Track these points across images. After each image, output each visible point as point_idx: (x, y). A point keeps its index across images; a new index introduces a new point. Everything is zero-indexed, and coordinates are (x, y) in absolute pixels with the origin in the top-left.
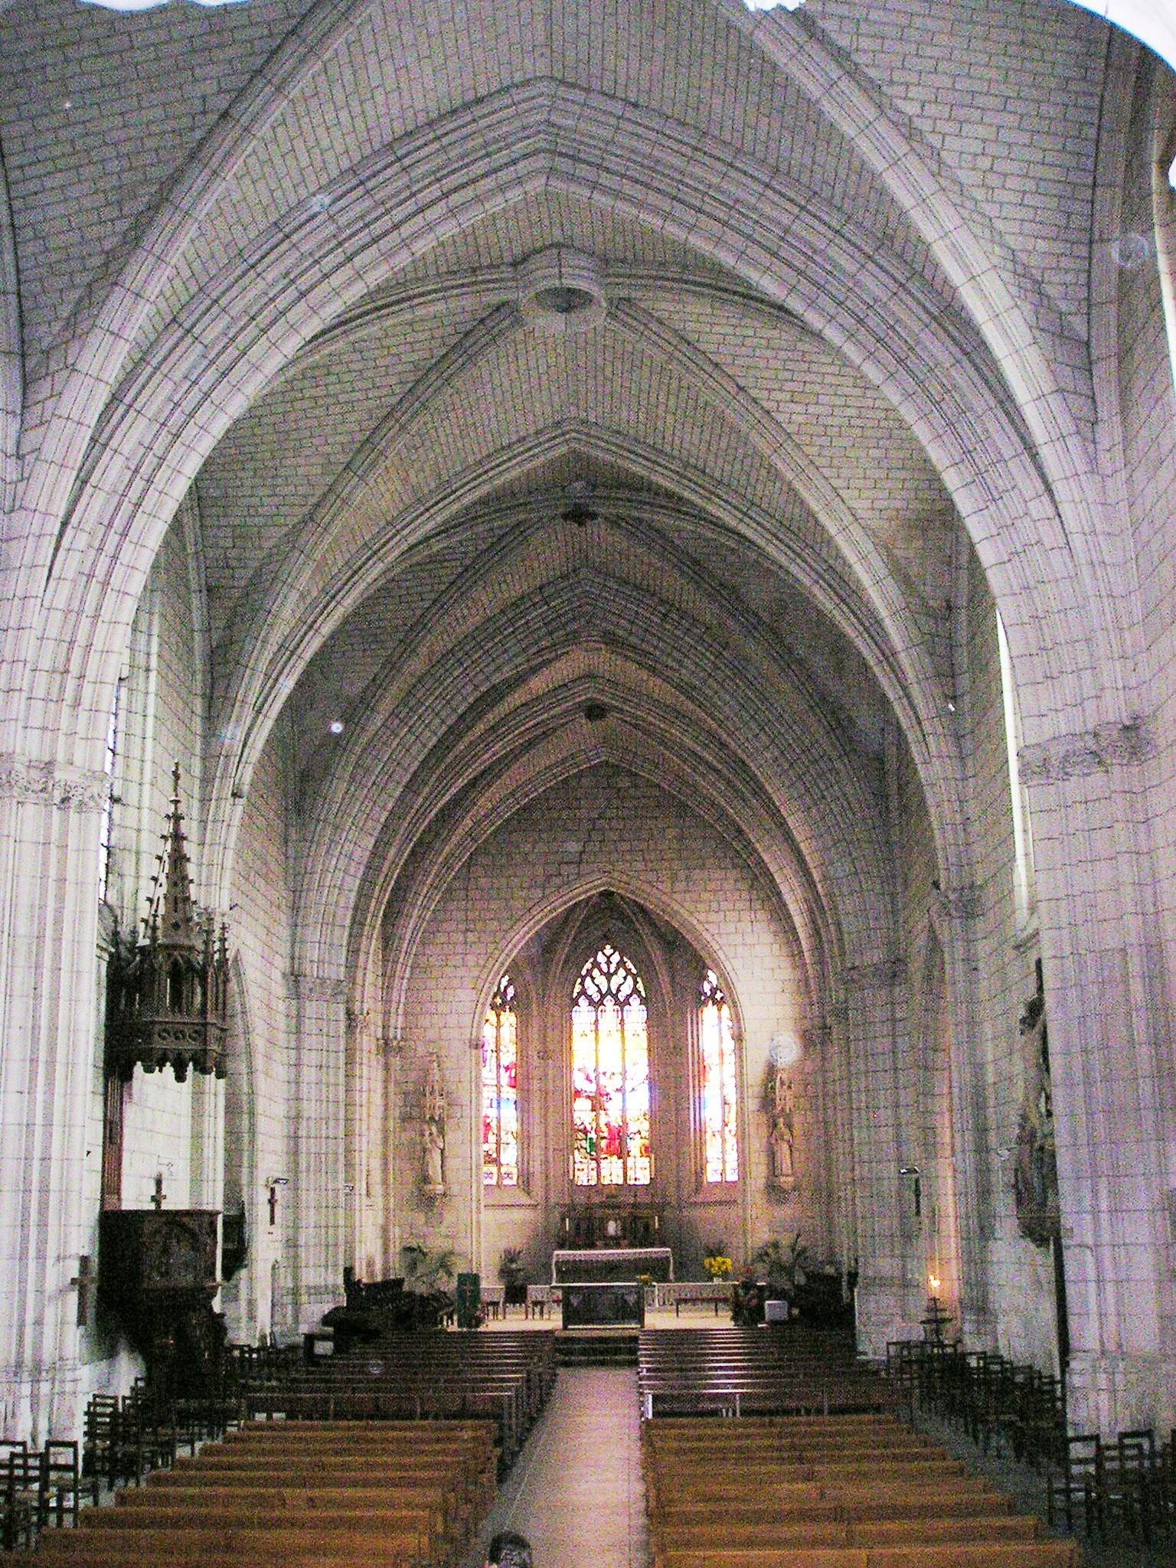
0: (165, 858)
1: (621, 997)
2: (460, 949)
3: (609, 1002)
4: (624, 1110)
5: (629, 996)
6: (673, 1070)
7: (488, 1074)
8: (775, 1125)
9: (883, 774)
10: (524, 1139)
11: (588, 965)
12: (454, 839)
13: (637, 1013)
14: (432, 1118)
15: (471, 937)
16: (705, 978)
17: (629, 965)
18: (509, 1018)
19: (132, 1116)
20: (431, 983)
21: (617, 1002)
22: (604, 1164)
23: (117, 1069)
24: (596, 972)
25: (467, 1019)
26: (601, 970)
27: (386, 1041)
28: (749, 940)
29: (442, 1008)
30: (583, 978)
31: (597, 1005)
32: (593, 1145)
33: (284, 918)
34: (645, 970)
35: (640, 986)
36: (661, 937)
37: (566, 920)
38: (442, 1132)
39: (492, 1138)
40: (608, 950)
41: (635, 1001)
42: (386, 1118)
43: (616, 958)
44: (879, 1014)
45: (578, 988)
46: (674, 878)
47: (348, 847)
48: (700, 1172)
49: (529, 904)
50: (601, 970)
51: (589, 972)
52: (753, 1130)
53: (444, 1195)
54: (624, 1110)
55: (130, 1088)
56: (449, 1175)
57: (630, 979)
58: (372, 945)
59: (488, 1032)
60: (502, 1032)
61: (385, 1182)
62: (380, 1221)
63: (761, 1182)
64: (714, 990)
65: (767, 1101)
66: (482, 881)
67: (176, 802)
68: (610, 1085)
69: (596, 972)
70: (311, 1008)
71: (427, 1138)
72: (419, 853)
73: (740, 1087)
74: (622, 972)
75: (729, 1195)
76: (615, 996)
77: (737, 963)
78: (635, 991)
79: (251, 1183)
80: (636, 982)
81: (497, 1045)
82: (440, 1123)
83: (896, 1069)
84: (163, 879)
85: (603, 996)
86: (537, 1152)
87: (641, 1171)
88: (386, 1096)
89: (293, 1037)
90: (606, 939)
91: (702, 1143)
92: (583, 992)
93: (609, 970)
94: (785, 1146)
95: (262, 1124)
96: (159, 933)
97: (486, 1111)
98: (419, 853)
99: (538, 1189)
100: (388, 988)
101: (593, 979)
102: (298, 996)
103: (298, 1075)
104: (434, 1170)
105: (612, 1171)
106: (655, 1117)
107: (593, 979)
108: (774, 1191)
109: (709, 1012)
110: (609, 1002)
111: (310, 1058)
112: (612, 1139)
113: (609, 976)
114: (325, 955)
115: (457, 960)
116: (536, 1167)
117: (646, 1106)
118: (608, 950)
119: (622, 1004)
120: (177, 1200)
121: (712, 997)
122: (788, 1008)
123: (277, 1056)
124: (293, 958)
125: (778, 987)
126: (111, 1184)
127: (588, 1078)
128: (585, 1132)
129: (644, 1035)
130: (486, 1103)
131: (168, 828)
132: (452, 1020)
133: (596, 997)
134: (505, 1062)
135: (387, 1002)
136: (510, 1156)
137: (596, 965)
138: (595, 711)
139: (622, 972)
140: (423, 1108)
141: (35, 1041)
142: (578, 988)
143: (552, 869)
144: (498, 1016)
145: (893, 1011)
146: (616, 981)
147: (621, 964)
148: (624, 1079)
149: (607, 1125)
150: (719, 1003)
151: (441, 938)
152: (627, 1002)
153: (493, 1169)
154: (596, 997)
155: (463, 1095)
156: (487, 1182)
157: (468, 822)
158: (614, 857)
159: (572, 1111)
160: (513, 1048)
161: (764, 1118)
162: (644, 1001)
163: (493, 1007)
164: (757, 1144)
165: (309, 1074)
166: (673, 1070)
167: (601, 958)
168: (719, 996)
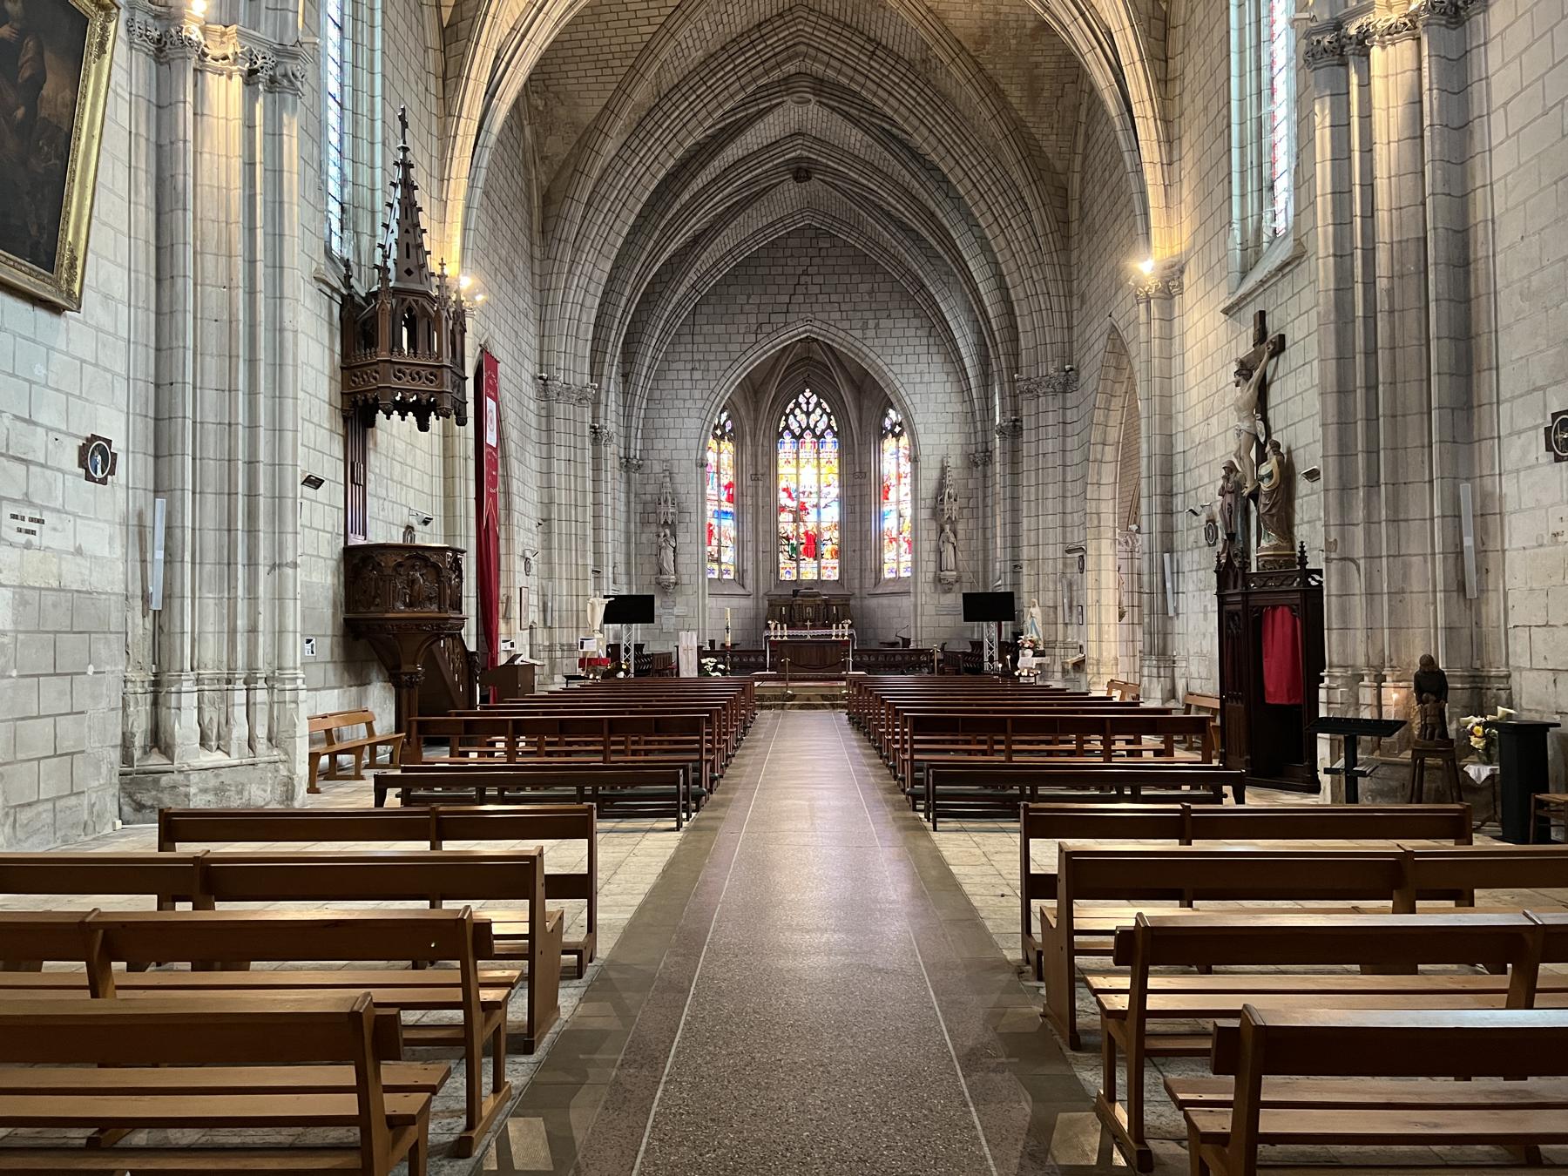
0: (396, 205)
2: (689, 347)
3: (808, 437)
4: (819, 522)
7: (711, 490)
8: (942, 530)
9: (1065, 206)
10: (740, 544)
11: (791, 405)
12: (682, 290)
13: (830, 445)
15: (697, 375)
16: (887, 415)
17: (825, 405)
18: (728, 447)
19: (376, 462)
20: (664, 413)
21: (814, 435)
22: (802, 564)
23: (357, 416)
24: (797, 411)
25: (695, 442)
27: (628, 459)
28: (926, 378)
30: (787, 416)
31: (798, 438)
32: (794, 549)
33: (532, 329)
34: (838, 411)
35: (833, 423)
36: (851, 380)
37: (774, 366)
38: (674, 535)
39: (714, 542)
40: (808, 393)
41: (829, 438)
42: (628, 521)
43: (814, 399)
44: (1051, 418)
45: (783, 424)
46: (864, 328)
47: (589, 268)
48: (879, 571)
49: (745, 347)
51: (792, 411)
52: (924, 534)
54: (819, 522)
55: (374, 436)
56: (681, 569)
58: (612, 371)
59: (711, 457)
60: (722, 456)
61: (628, 573)
63: (931, 575)
64: (894, 425)
65: (937, 512)
66: (706, 329)
67: (405, 150)
68: (810, 502)
69: (797, 411)
70: (560, 409)
71: (662, 539)
72: (649, 301)
73: (915, 500)
74: (819, 411)
75: (901, 589)
76: (813, 431)
77: (916, 399)
78: (829, 427)
79: (508, 554)
81: (718, 467)
82: (672, 526)
83: (1064, 466)
84: (394, 225)
85: (803, 431)
86: (749, 554)
87: (831, 570)
88: (628, 503)
89: (544, 434)
92: (787, 427)
93: (809, 411)
95: (517, 502)
96: (392, 275)
97: (708, 520)
98: (649, 301)
99: (749, 582)
100: (628, 416)
102: (547, 398)
103: (549, 466)
104: (668, 564)
106: (841, 526)
109: (889, 444)
110: (808, 437)
111: (560, 453)
113: (808, 414)
114: (573, 368)
115: (684, 394)
116: (749, 566)
117: (837, 519)
118: (808, 393)
120: (429, 538)
121: (892, 431)
123: (529, 448)
124: (541, 351)
125: (949, 418)
126: (355, 515)
127: (790, 496)
128: (788, 539)
129: (836, 463)
130: (709, 514)
131: (398, 174)
132: (681, 443)
134: (725, 481)
135: (628, 427)
136: (728, 556)
137: (798, 405)
138: (802, 172)
139: (819, 411)
140: (658, 516)
141: (232, 334)
142: (783, 424)
143: (763, 318)
145: (1064, 415)
146: (814, 418)
147: (818, 404)
149: (806, 533)
150: (897, 436)
151: (671, 375)
152: (822, 436)
153: (715, 566)
155: (691, 504)
157: (692, 276)
158: (816, 308)
159: (777, 522)
160: (731, 472)
161: (933, 525)
162: (836, 434)
163: (715, 436)
164: (927, 546)
165: (558, 466)
167: (801, 399)
168: (897, 429)
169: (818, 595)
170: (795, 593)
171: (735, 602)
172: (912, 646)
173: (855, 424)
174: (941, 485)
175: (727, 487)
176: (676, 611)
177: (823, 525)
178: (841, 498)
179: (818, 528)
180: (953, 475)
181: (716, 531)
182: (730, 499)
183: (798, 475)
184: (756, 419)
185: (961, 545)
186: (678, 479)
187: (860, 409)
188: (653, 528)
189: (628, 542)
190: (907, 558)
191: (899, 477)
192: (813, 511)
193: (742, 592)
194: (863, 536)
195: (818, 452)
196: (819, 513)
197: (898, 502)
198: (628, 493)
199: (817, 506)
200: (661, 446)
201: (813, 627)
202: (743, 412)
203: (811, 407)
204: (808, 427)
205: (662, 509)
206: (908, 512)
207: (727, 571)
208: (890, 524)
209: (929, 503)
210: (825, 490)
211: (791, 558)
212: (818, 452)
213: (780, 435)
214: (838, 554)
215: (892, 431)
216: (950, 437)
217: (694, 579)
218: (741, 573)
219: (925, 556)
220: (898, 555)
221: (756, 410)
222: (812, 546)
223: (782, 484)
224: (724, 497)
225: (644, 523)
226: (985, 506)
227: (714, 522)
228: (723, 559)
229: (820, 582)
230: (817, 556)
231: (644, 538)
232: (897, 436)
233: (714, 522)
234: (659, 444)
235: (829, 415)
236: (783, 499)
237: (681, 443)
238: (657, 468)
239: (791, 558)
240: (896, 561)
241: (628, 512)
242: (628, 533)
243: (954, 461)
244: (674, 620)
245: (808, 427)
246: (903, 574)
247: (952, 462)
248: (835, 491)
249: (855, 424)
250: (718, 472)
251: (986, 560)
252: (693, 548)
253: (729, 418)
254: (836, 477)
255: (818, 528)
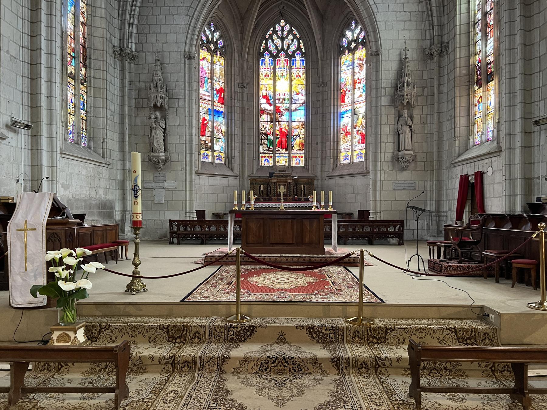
1: (290, 52)
3: (282, 57)
4: (290, 121)
5: (294, 52)
6: (322, 95)
8: (400, 116)
10: (229, 136)
11: (270, 32)
14: (155, 106)
17: (295, 32)
18: (219, 60)
20: (157, 11)
21: (287, 55)
24: (275, 37)
25: (182, 37)
26: (277, 35)
29: (164, 29)
30: (267, 40)
31: (274, 57)
32: (271, 142)
34: (306, 36)
38: (164, 118)
39: (208, 134)
40: (282, 23)
41: (298, 58)
42: (122, 105)
43: (288, 27)
50: (277, 35)
51: (271, 37)
52: (384, 118)
53: (166, 161)
54: (290, 121)
57: (295, 42)
62: (119, 177)
63: (389, 156)
64: (350, 43)
74: (291, 37)
75: (361, 171)
76: (286, 52)
78: (299, 48)
80: (299, 43)
85: (279, 52)
86: (236, 145)
87: (299, 158)
88: (122, 89)
90: (282, 15)
91: (337, 142)
92: (267, 49)
94: (408, 130)
99: (236, 166)
101: (273, 41)
105: (282, 159)
106: (307, 125)
107: (273, 41)
108: (399, 162)
109: (346, 58)
110: (282, 57)
112: (281, 139)
113: (282, 39)
116: (236, 154)
117: (303, 120)
118: (282, 23)
119: (291, 57)
121: (349, 48)
122: (413, 33)
125: (406, 16)
127: (268, 102)
128: (267, 134)
130: (203, 111)
132: (171, 38)
133: (274, 52)
134: (217, 86)
136: (219, 146)
137: (275, 32)
139: (291, 37)
144: (212, 56)
146: (287, 42)
147: (290, 32)
148: (291, 103)
149: (280, 130)
152: (293, 55)
154: (274, 52)
155: (180, 90)
156: (205, 160)
159: (258, 122)
160: (222, 80)
161: (392, 111)
162: (303, 55)
163: (209, 50)
166: (322, 95)
167: (278, 27)
169: (289, 175)
170: (272, 174)
171: (224, 181)
172: (371, 217)
173: (319, 44)
174: (400, 74)
175: (220, 91)
176: (166, 185)
177: (294, 124)
178: (307, 104)
179: (290, 126)
180: (411, 67)
181: (209, 125)
182: (221, 101)
183: (274, 85)
184: (242, 41)
185: (416, 128)
186: (169, 69)
187: (323, 33)
188: (146, 111)
189: (122, 123)
190: (360, 147)
191: (354, 83)
192: (287, 113)
193: (230, 173)
194: (325, 132)
195: (290, 68)
196: (290, 116)
197: (353, 103)
198: (123, 79)
199: (289, 110)
200: (153, 40)
201: (286, 201)
202: (232, 33)
203: (285, 33)
204: (283, 49)
205: (153, 93)
206: (362, 109)
207: (219, 157)
208: (346, 121)
209: (389, 91)
210: (295, 98)
211: (268, 149)
212: (290, 68)
213: (261, 55)
214: (304, 146)
215: (349, 48)
216: (407, 33)
217: (182, 157)
218: (230, 159)
219: (384, 138)
220: (352, 145)
221: (243, 33)
222: (285, 141)
223: (263, 93)
224: (216, 99)
225: (139, 107)
226: (440, 93)
227: (207, 117)
228: (216, 147)
229: (290, 167)
230: (288, 148)
231: (138, 121)
232: (353, 51)
233: (207, 117)
234: (152, 39)
235: (298, 40)
236: (264, 104)
237: (171, 38)
238: (150, 59)
239: (268, 149)
240: (351, 150)
241: (123, 96)
242: (122, 116)
243: (412, 55)
244: (164, 193)
245: (283, 49)
246: (355, 160)
247: (409, 54)
248: (302, 98)
249: (319, 44)
250: (212, 79)
251: (440, 141)
252: (181, 130)
253: (221, 37)
254: (303, 87)
255: (290, 126)
